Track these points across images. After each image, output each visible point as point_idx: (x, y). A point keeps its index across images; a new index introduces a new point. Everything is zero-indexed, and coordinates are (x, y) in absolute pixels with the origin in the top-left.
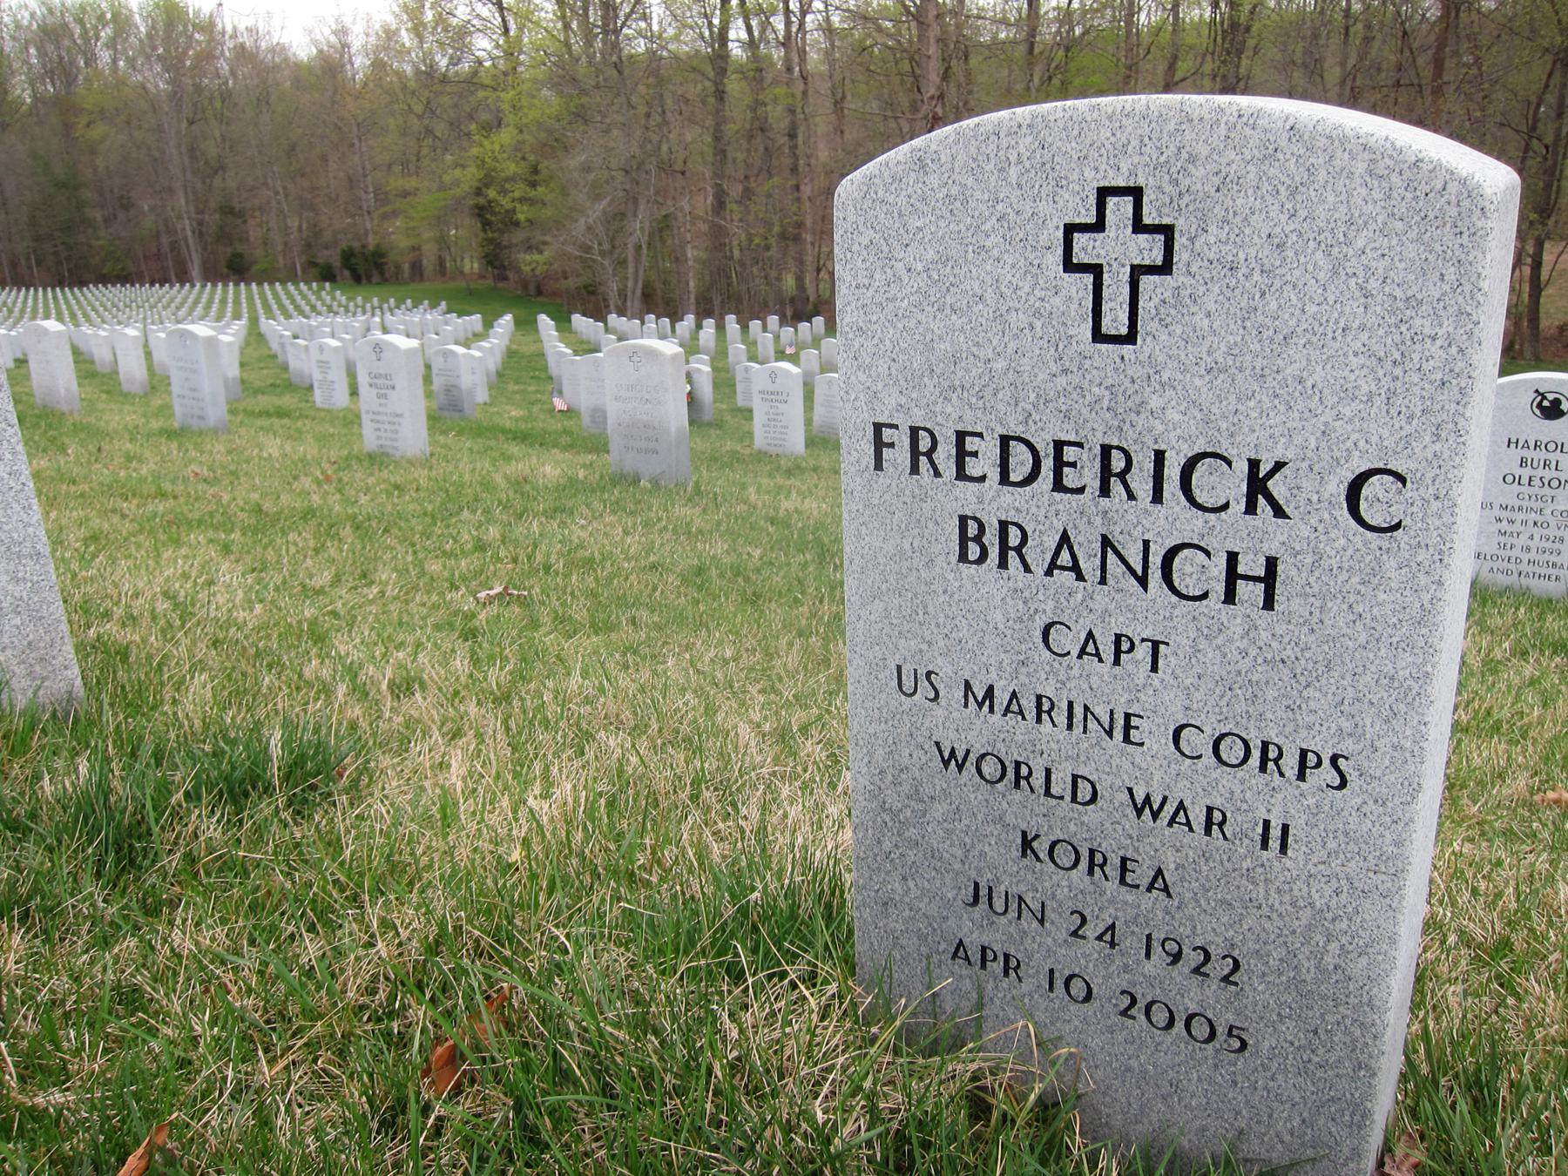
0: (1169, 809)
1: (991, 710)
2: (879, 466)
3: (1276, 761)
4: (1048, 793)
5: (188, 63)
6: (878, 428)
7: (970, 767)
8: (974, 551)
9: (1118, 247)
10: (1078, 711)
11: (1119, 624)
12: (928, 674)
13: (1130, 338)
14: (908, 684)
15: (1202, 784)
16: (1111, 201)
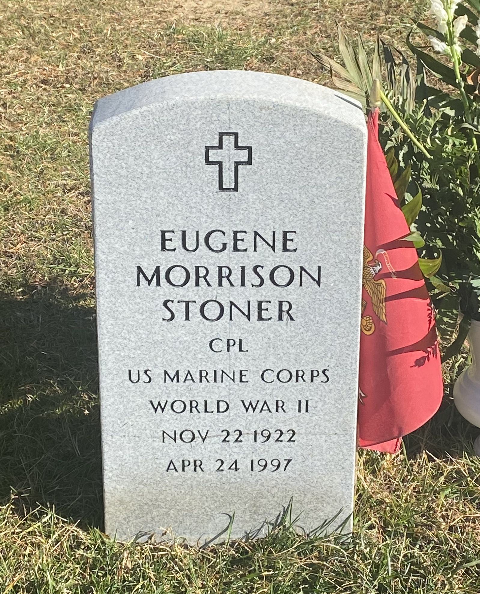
0: (260, 406)
1: (178, 381)
3: (228, 277)
4: (206, 411)
7: (168, 407)
10: (219, 373)
11: (220, 367)
12: (146, 372)
13: (236, 189)
14: (134, 378)
15: (273, 392)
16: (225, 138)
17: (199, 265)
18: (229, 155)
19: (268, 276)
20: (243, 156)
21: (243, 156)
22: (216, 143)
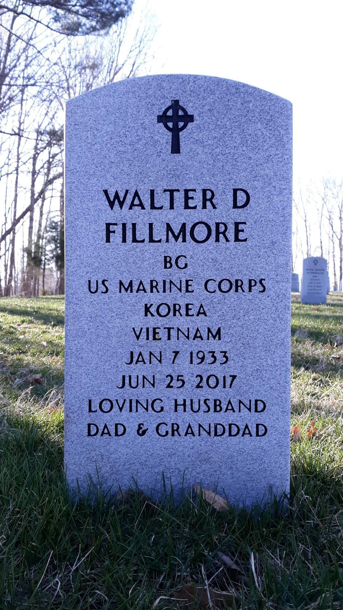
2: (108, 240)
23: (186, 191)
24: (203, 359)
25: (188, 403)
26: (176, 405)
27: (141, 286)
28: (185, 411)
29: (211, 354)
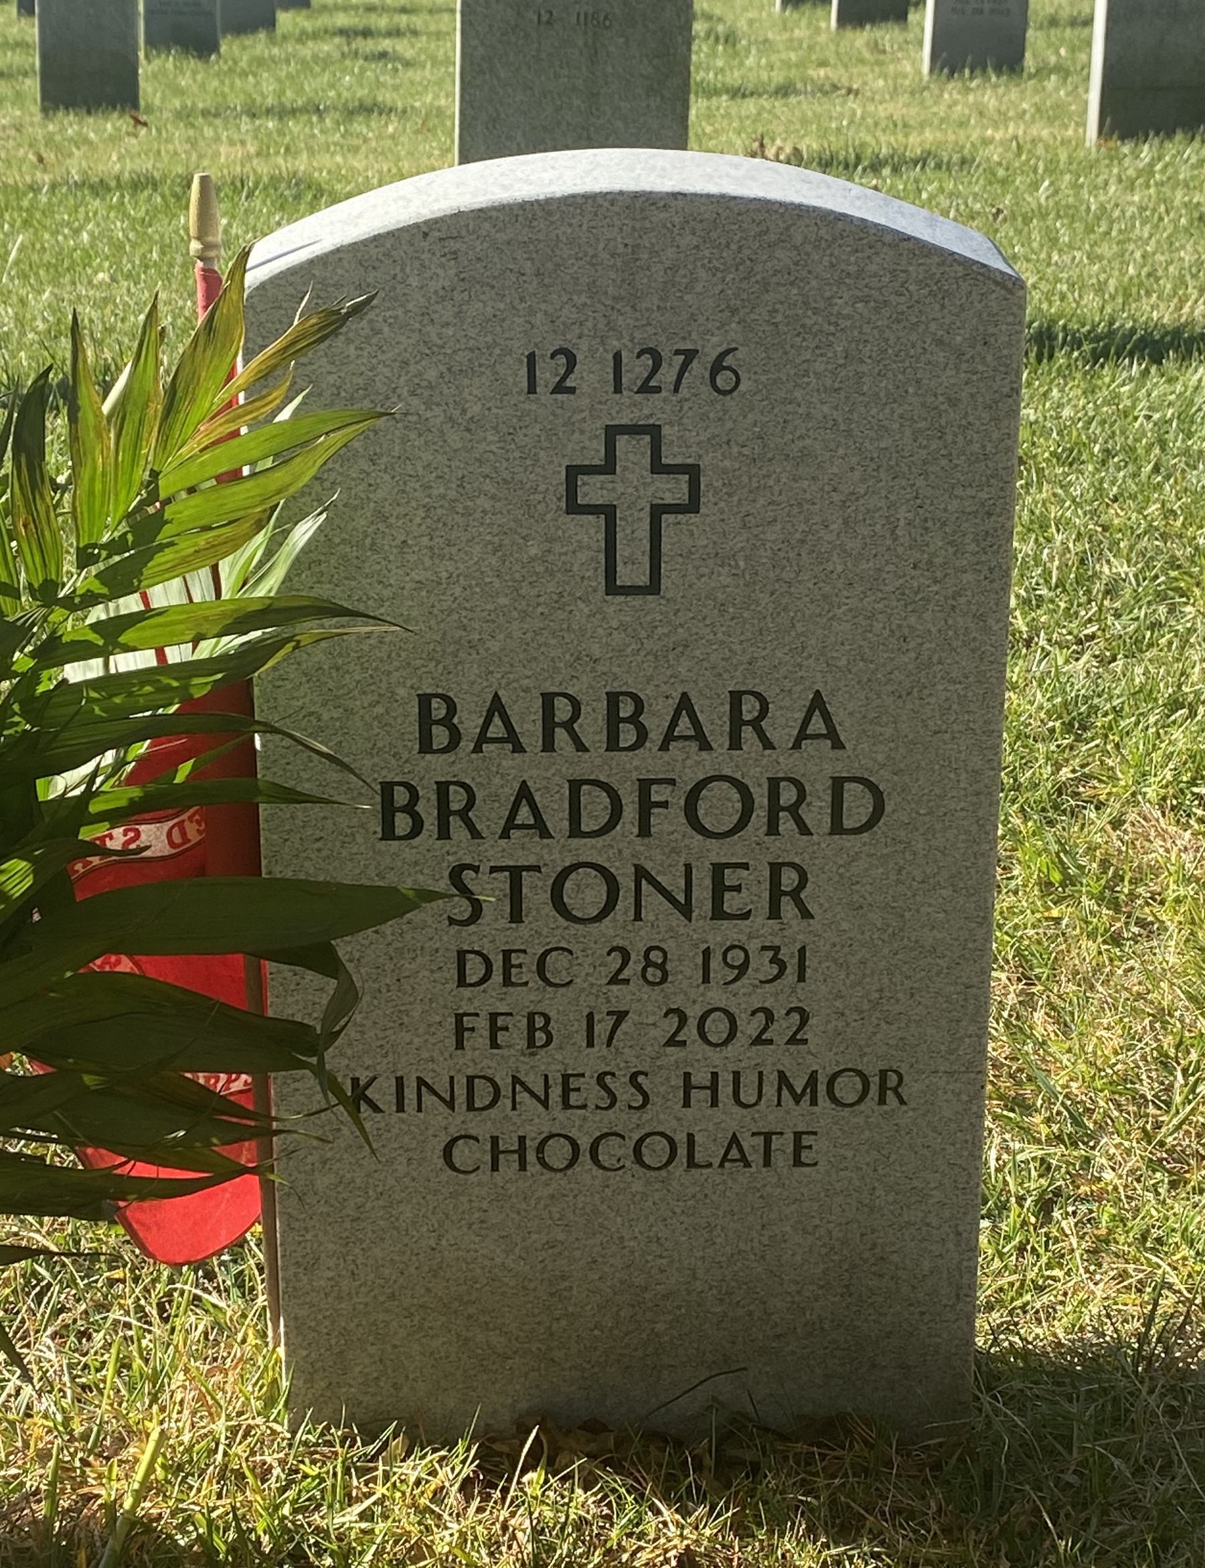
2: (460, 1045)
5: (189, 1075)
6: (459, 1018)
8: (402, 823)
9: (634, 487)
13: (654, 587)
16: (622, 442)
17: (466, 948)
18: (634, 487)
19: (581, 1159)
20: (674, 490)
21: (674, 490)
22: (596, 456)
23: (493, 1017)
24: (743, 968)
25: (726, 1079)
26: (688, 1086)
27: (497, 720)
28: (714, 1103)
29: (771, 954)
